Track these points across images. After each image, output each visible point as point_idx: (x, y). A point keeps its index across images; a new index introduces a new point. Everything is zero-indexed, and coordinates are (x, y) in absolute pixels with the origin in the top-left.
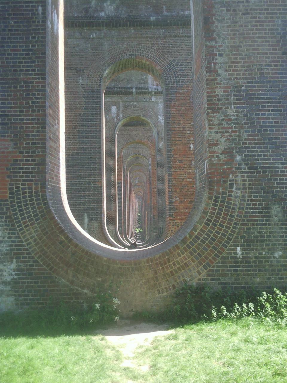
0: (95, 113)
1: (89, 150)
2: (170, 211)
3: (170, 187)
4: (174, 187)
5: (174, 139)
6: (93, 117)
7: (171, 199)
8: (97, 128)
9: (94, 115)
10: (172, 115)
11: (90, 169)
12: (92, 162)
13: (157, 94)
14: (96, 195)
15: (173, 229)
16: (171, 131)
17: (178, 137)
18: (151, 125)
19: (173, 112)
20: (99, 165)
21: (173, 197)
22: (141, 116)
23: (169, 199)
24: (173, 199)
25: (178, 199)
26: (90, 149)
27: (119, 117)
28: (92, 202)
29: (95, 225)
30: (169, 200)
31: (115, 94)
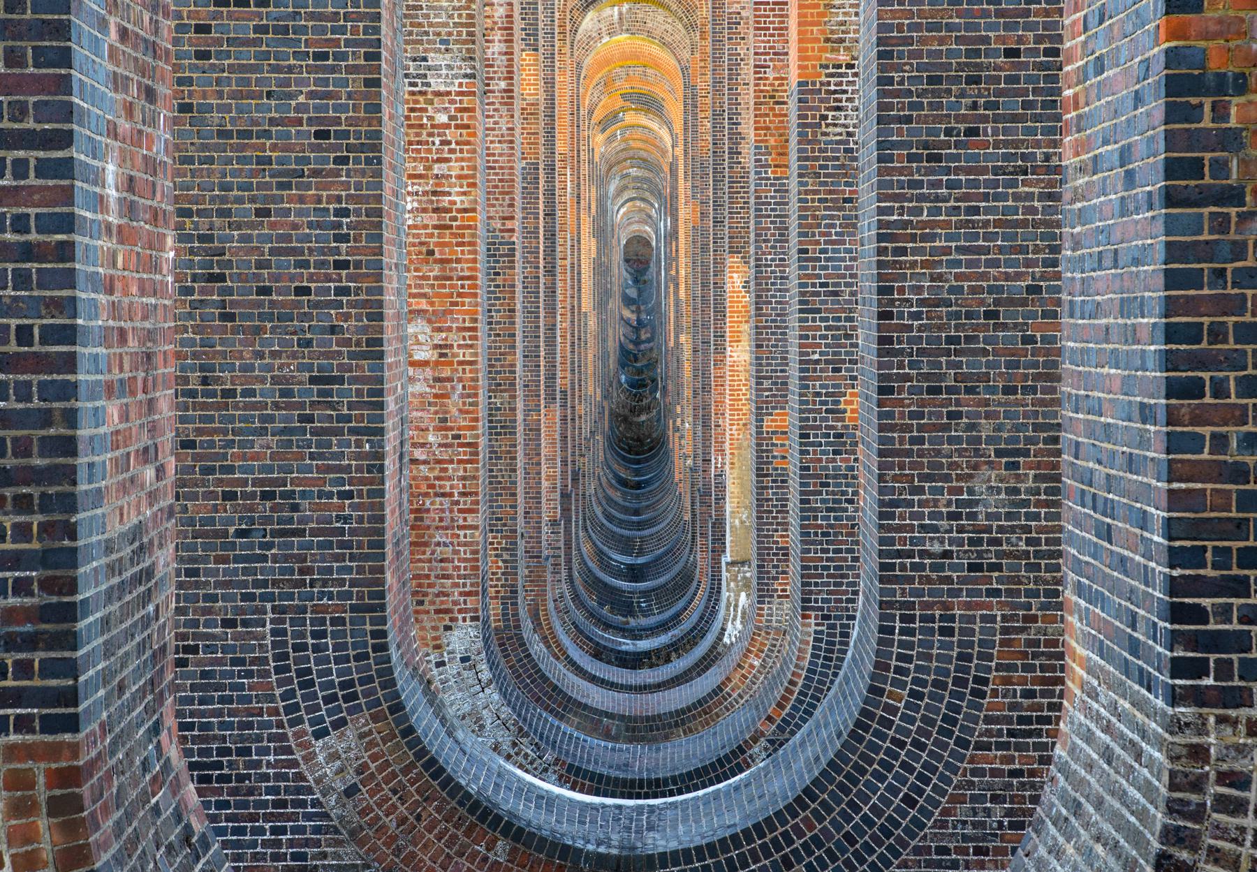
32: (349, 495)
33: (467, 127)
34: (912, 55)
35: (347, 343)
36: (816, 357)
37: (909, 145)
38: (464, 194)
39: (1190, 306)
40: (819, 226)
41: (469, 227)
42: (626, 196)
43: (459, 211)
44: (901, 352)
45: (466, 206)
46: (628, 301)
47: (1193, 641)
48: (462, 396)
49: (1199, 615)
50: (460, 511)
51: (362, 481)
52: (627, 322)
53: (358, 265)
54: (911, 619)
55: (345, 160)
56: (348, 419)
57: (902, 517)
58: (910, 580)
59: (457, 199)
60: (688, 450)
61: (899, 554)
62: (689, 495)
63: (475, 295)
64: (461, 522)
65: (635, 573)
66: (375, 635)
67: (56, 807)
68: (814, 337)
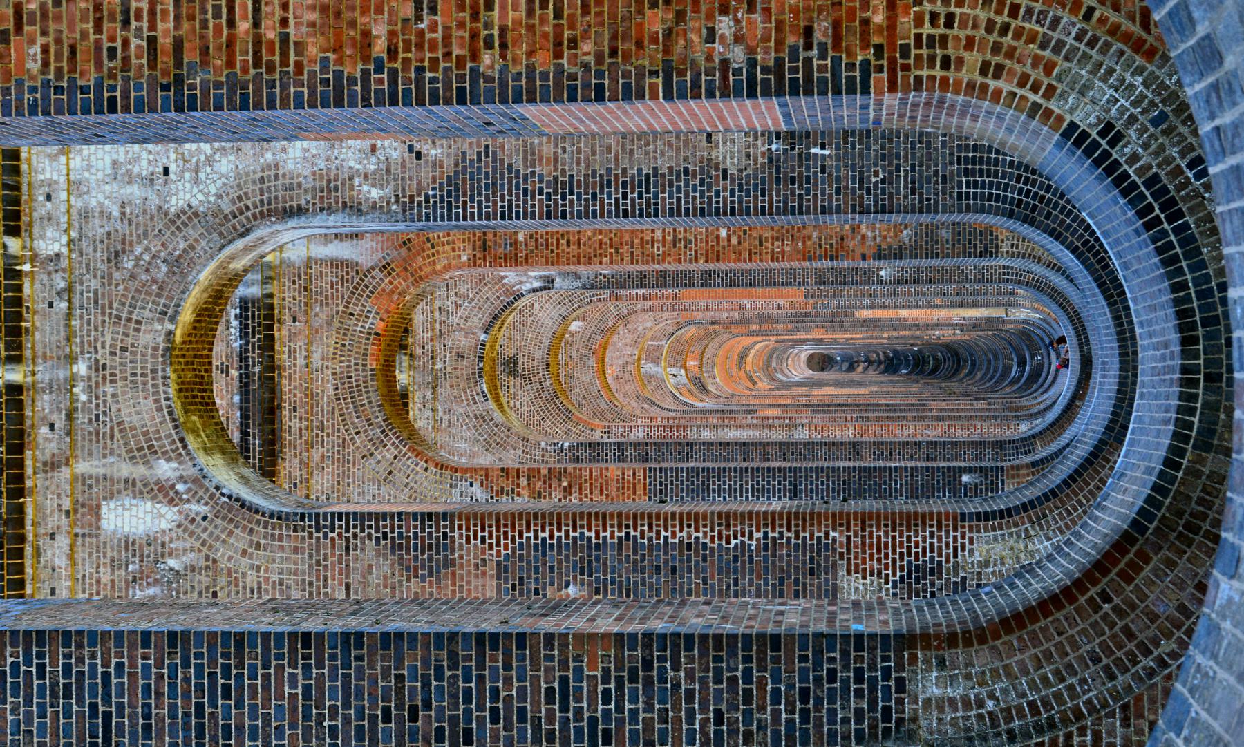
0: (41, 675)
1: (333, 729)
3: (627, 86)
4: (627, 56)
5: (244, 56)
6: (68, 695)
7: (725, 78)
8: (160, 664)
9: (54, 685)
10: (59, 71)
11: (481, 721)
12: (427, 706)
13: (16, 216)
14: (690, 676)
15: (973, 58)
16: (179, 80)
17: (231, 23)
18: (232, 258)
19: (34, 66)
20: (453, 656)
21: (709, 58)
22: (170, 333)
23: (725, 95)
24: (725, 63)
25: (725, 26)
26: (320, 718)
27: (181, 479)
28: (748, 714)
29: (935, 691)
31: (21, 509)
42: (786, 371)
52: (866, 369)
65: (1022, 363)
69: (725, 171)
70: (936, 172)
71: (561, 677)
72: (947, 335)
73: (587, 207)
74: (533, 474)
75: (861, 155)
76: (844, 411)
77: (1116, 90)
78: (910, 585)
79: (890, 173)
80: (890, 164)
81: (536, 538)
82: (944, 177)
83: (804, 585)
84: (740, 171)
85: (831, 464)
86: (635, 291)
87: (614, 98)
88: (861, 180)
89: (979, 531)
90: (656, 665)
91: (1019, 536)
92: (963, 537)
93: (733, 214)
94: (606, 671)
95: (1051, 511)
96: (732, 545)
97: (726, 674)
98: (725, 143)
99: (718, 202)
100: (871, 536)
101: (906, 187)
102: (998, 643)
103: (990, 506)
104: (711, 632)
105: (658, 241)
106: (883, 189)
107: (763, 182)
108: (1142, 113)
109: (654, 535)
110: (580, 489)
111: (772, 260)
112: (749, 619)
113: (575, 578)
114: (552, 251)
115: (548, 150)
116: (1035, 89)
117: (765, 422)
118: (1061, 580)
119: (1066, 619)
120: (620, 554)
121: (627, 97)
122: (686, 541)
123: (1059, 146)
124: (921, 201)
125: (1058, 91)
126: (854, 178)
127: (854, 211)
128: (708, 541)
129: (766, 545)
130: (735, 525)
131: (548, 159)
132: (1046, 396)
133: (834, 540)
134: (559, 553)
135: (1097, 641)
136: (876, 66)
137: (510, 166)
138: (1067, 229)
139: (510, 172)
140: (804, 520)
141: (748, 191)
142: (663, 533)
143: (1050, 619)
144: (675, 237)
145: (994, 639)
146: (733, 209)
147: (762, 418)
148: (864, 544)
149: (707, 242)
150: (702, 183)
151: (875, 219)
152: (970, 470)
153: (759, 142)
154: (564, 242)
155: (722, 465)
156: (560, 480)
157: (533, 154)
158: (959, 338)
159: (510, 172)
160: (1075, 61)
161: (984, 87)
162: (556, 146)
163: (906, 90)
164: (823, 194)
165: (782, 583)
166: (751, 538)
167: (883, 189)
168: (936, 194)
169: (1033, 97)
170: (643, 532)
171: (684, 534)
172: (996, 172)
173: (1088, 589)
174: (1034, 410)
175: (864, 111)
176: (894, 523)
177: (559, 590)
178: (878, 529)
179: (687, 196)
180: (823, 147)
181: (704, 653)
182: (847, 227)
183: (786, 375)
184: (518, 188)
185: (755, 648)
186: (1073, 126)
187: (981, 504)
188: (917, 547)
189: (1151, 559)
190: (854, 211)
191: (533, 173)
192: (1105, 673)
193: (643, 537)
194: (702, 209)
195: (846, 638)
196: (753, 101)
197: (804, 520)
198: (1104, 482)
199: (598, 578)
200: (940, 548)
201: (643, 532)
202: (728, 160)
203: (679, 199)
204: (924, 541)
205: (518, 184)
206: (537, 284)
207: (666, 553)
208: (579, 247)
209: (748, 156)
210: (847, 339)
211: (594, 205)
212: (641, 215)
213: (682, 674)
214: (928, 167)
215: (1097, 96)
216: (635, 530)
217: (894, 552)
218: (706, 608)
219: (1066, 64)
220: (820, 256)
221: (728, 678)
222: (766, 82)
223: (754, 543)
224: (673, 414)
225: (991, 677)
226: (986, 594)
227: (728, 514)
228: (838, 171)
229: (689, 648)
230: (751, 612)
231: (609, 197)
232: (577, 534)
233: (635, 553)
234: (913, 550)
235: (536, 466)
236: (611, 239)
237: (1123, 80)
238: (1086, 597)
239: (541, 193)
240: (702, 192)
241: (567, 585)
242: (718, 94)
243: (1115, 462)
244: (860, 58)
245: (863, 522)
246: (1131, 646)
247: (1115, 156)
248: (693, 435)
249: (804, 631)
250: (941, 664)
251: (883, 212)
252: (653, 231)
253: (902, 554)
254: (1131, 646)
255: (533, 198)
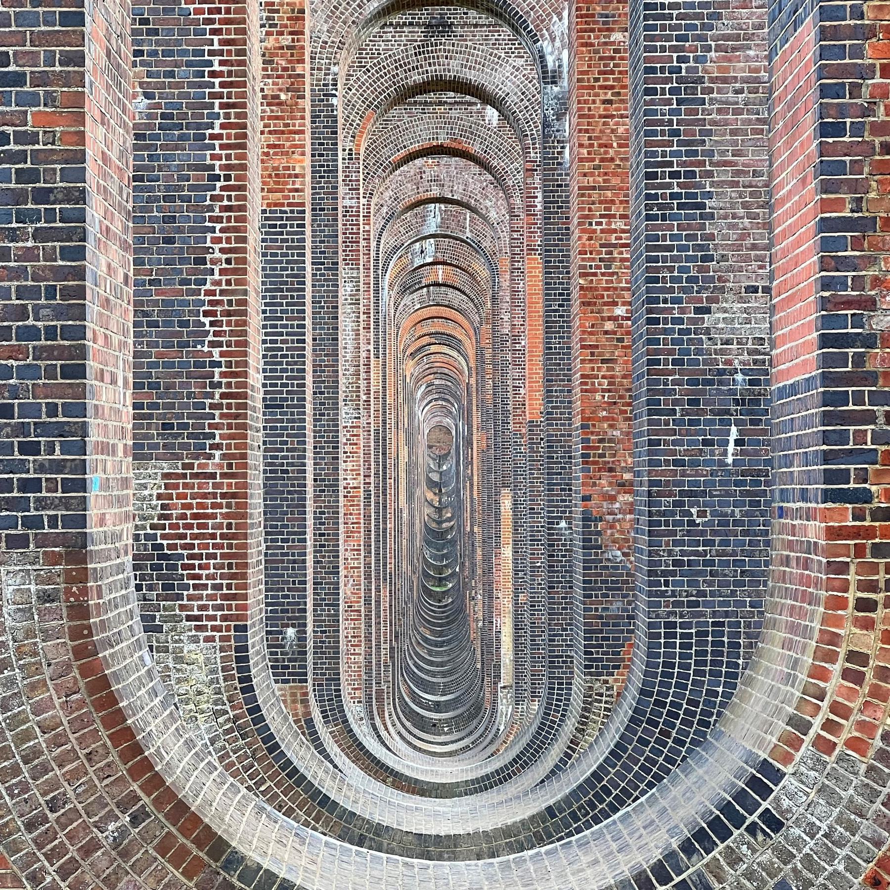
2: (843, 438)
7: (849, 303)
14: (29, 255)
23: (824, 303)
30: (826, 322)
32: (325, 632)
33: (356, 444)
34: (561, 447)
35: (324, 568)
36: (539, 564)
37: (560, 484)
38: (354, 479)
39: (589, 575)
40: (540, 496)
41: (357, 497)
43: (351, 488)
44: (557, 571)
45: (355, 485)
46: (431, 484)
47: (590, 660)
48: (353, 585)
49: (591, 653)
50: (352, 645)
51: (330, 626)
53: (329, 535)
54: (562, 684)
55: (324, 491)
56: (324, 600)
57: (558, 641)
58: (562, 667)
59: (351, 482)
60: (480, 615)
61: (557, 657)
62: (479, 649)
63: (359, 532)
64: (352, 651)
66: (336, 691)
67: (302, 701)
68: (538, 554)
69: (708, 311)
70: (703, 594)
71: (24, 74)
72: (477, 609)
73: (661, 123)
74: (295, 53)
75: (728, 494)
76: (377, 474)
77: (826, 836)
78: (151, 557)
79: (703, 533)
80: (714, 533)
81: (212, 53)
82: (696, 604)
83: (150, 417)
84: (707, 331)
85: (310, 454)
86: (540, 195)
87: (823, 149)
88: (691, 494)
89: (222, 649)
90: (42, 207)
91: (216, 703)
92: (214, 628)
93: (650, 321)
94: (33, 139)
95: (248, 745)
96: (202, 319)
97: (30, 304)
98: (745, 310)
99: (665, 301)
100: (215, 506)
101: (683, 553)
102: (76, 673)
103: (256, 664)
104: (88, 284)
105: (609, 224)
106: (680, 523)
107: (691, 362)
108: (795, 870)
109: (217, 213)
110: (277, 118)
111: (582, 376)
112: (106, 336)
113: (158, 106)
114: (597, 80)
115: (740, 69)
116: (829, 726)
117: (362, 368)
118: (162, 758)
119: (108, 765)
120: (190, 167)
121: (824, 168)
122: (208, 256)
123: (749, 758)
124: (664, 573)
125: (826, 758)
126: (697, 484)
127: (651, 483)
128: (208, 286)
129: (203, 365)
130: (229, 323)
131: (726, 69)
132: (397, 738)
133: (210, 457)
134: (191, 85)
135: (79, 807)
136: (862, 510)
137: (719, 17)
138: (625, 766)
139: (710, 16)
140: (237, 416)
141: (679, 342)
142: (218, 226)
143: (109, 743)
144: (615, 246)
145: (80, 668)
146: (657, 321)
147: (368, 364)
148: (205, 496)
149: (607, 289)
150: (692, 280)
151: (640, 513)
152: (301, 637)
153: (746, 357)
154: (609, 96)
155: (308, 309)
156: (288, 90)
157: (735, 49)
158: (473, 625)
159: (710, 16)
160: (867, 781)
161: (831, 657)
162: (745, 80)
163: (829, 552)
164: (674, 443)
165: (151, 386)
166: (212, 344)
167: (680, 523)
168: (673, 594)
169: (817, 723)
170: (220, 198)
171: (217, 255)
172: (702, 673)
173: (149, 795)
174: (378, 722)
175: (797, 495)
176: (234, 536)
177: (141, 84)
178: (226, 516)
179: (674, 259)
180: (738, 442)
181: (60, 273)
182: (627, 476)
183: (423, 398)
184: (688, 27)
185: (66, 343)
186: (777, 776)
187: (258, 653)
188: (201, 567)
189: (190, 879)
190: (651, 483)
191: (708, 49)
192: (36, 817)
193: (213, 198)
194: (656, 280)
195: (82, 467)
196: (816, 343)
197: (237, 416)
198: (288, 813)
199: (157, 137)
200: (200, 598)
201: (220, 198)
202: (721, 315)
203: (670, 248)
204: (208, 577)
205: (695, 27)
206: (550, 61)
207: (192, 230)
208: (601, 117)
209: (728, 342)
210: (471, 479)
211: (663, 133)
212: (648, 197)
213: (30, 244)
214: (710, 584)
215: (819, 809)
216: (223, 189)
217: (195, 537)
218: (121, 278)
219: (863, 768)
220: (588, 440)
221: (25, 306)
222: (843, 360)
223: (206, 349)
224: (373, 244)
225: (30, 664)
226: (141, 658)
227: (244, 313)
228: (706, 463)
229: (66, 254)
230: (116, 339)
231: (673, 154)
232: (217, 110)
233: (192, 188)
234: (197, 562)
235: (307, 58)
236: (612, 160)
237: (841, 846)
238: (140, 793)
239: (680, 60)
240: (678, 280)
241: (147, 96)
242: (826, 294)
243: (315, 829)
244: (874, 488)
245: (234, 496)
246: (72, 852)
247: (736, 833)
248: (343, 271)
249: (90, 411)
250: (46, 597)
251: (651, 524)
252: (623, 217)
253: (192, 546)
254: (72, 852)
255: (674, 49)
